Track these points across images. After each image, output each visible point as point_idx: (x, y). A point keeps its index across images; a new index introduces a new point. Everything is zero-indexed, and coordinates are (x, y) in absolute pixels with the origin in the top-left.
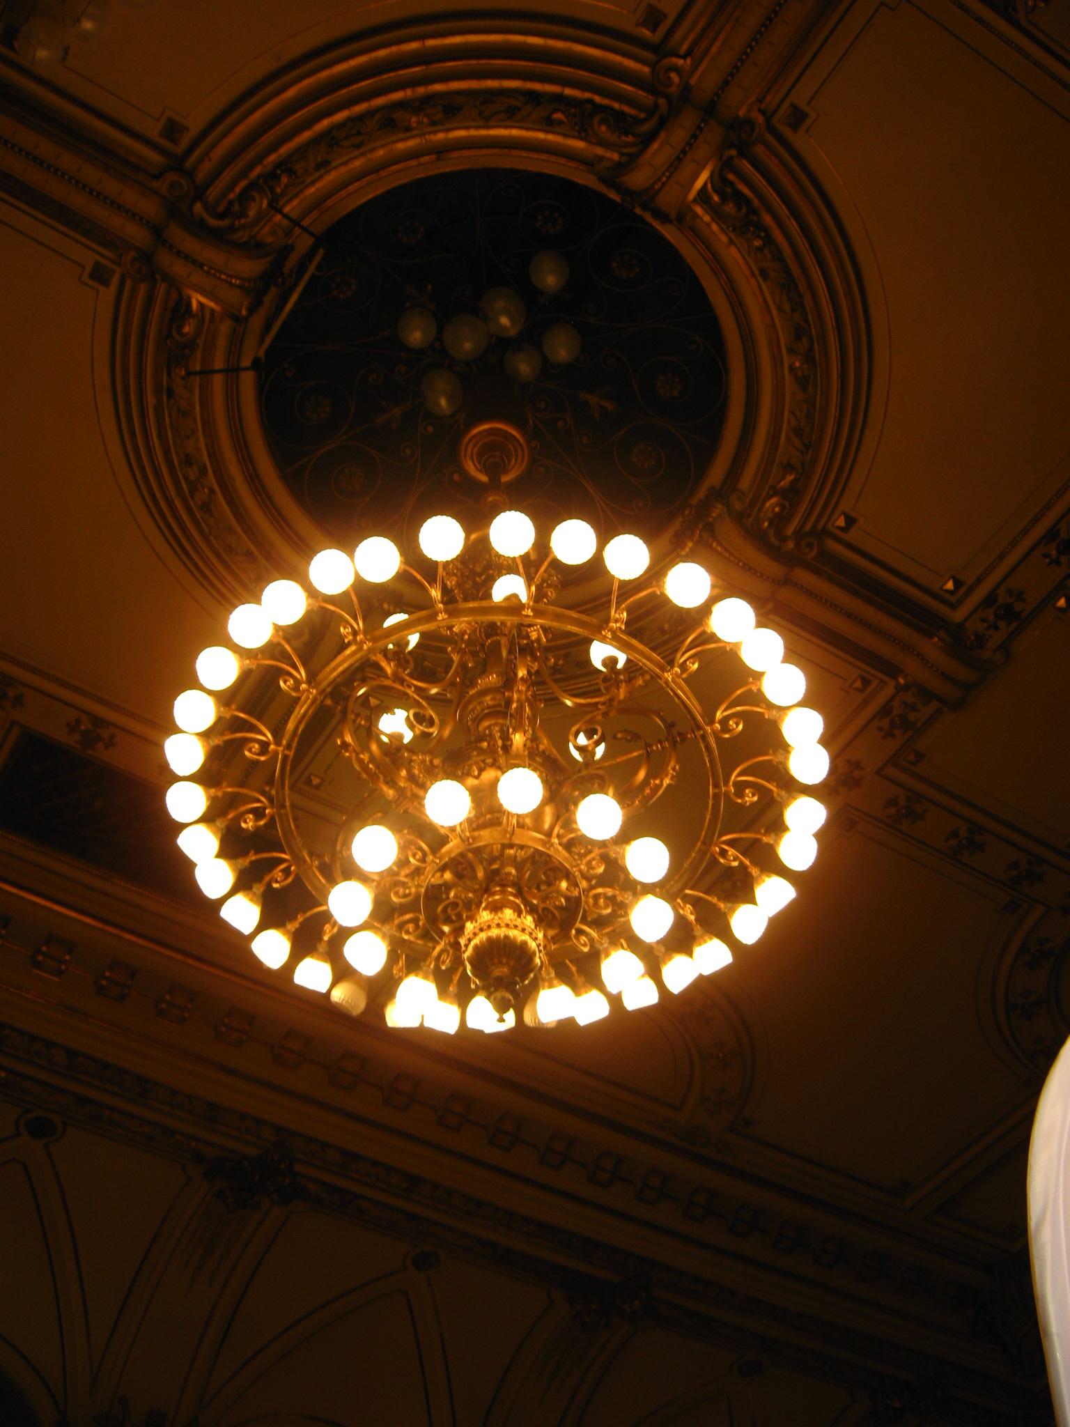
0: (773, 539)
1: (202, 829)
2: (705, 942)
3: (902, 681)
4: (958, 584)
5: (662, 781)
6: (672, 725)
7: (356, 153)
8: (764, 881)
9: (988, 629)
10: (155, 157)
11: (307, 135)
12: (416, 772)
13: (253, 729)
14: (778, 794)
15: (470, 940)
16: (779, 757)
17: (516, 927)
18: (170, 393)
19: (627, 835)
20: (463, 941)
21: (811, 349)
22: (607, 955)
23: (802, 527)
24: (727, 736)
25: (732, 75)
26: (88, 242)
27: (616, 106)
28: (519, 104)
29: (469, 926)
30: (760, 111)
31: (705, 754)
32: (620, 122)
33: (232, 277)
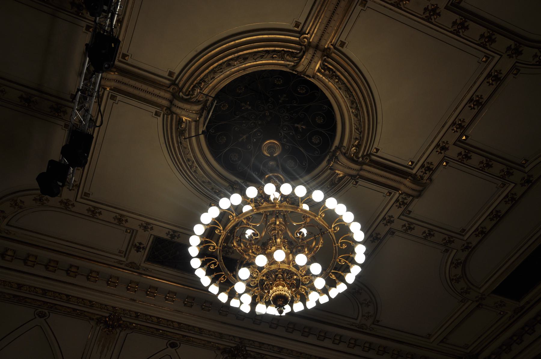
0: (355, 158)
1: (201, 269)
2: (339, 284)
3: (400, 192)
4: (412, 163)
5: (319, 246)
6: (321, 229)
7: (221, 73)
8: (352, 267)
9: (423, 174)
10: (168, 82)
11: (207, 71)
12: (254, 250)
13: (211, 243)
14: (352, 244)
15: (271, 295)
16: (350, 235)
17: (283, 290)
18: (181, 143)
19: (309, 263)
20: (270, 295)
21: (357, 106)
22: (310, 293)
23: (363, 154)
24: (335, 232)
25: (322, 37)
26: (152, 106)
27: (291, 50)
28: (264, 54)
29: (271, 291)
30: (331, 45)
31: (331, 236)
32: (292, 54)
33: (193, 111)
